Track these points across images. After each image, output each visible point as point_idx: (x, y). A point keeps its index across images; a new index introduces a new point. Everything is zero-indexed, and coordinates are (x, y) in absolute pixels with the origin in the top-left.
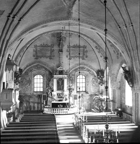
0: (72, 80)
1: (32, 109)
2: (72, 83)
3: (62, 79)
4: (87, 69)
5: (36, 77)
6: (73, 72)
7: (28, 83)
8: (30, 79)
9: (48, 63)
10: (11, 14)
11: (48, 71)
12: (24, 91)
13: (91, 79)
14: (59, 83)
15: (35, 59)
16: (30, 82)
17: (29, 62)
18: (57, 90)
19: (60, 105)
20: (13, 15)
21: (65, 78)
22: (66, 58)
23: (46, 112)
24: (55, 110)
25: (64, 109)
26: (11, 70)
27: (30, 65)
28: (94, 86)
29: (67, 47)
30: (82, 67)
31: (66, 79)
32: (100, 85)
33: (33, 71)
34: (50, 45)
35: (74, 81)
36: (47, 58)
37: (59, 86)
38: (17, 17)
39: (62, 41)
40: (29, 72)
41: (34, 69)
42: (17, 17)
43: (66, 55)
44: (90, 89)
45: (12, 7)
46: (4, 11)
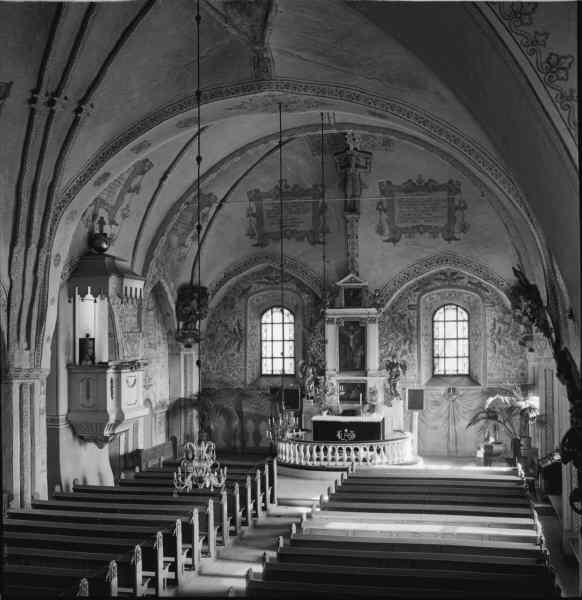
0: (407, 327)
1: (251, 443)
2: (408, 342)
3: (358, 322)
4: (469, 282)
5: (266, 318)
6: (410, 294)
7: (235, 341)
8: (243, 325)
9: (302, 259)
10: (36, 91)
11: (308, 293)
12: (219, 374)
13: (489, 325)
14: (349, 339)
16: (242, 337)
17: (232, 260)
18: (338, 369)
19: (343, 432)
20: (47, 95)
21: (373, 321)
22: (378, 236)
23: (288, 460)
24: (326, 450)
25: (361, 447)
27: (238, 271)
29: (378, 193)
30: (449, 274)
31: (377, 325)
32: (527, 349)
33: (252, 294)
34: (310, 186)
35: (415, 333)
36: (300, 239)
37: (345, 353)
38: (66, 98)
40: (237, 299)
41: (254, 285)
42: (66, 98)
44: (485, 366)
45: (37, 66)
46: (11, 83)
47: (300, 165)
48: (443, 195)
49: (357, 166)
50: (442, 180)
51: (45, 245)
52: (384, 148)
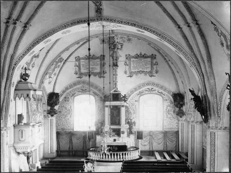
15: (77, 78)
21: (123, 106)
22: (125, 74)
26: (22, 97)
28: (170, 118)
38: (21, 22)
39: (116, 50)
40: (70, 98)
43: (124, 70)
47: (96, 48)
48: (149, 59)
49: (118, 48)
50: (149, 54)
51: (9, 79)
52: (128, 42)
